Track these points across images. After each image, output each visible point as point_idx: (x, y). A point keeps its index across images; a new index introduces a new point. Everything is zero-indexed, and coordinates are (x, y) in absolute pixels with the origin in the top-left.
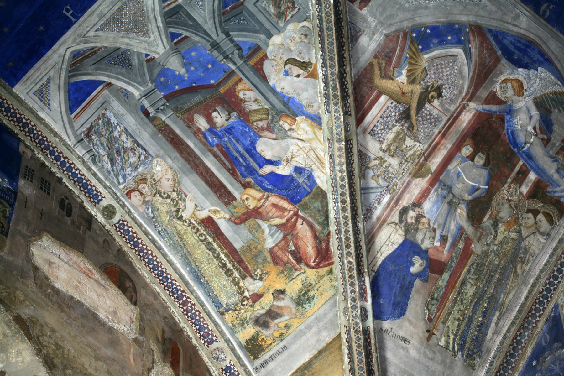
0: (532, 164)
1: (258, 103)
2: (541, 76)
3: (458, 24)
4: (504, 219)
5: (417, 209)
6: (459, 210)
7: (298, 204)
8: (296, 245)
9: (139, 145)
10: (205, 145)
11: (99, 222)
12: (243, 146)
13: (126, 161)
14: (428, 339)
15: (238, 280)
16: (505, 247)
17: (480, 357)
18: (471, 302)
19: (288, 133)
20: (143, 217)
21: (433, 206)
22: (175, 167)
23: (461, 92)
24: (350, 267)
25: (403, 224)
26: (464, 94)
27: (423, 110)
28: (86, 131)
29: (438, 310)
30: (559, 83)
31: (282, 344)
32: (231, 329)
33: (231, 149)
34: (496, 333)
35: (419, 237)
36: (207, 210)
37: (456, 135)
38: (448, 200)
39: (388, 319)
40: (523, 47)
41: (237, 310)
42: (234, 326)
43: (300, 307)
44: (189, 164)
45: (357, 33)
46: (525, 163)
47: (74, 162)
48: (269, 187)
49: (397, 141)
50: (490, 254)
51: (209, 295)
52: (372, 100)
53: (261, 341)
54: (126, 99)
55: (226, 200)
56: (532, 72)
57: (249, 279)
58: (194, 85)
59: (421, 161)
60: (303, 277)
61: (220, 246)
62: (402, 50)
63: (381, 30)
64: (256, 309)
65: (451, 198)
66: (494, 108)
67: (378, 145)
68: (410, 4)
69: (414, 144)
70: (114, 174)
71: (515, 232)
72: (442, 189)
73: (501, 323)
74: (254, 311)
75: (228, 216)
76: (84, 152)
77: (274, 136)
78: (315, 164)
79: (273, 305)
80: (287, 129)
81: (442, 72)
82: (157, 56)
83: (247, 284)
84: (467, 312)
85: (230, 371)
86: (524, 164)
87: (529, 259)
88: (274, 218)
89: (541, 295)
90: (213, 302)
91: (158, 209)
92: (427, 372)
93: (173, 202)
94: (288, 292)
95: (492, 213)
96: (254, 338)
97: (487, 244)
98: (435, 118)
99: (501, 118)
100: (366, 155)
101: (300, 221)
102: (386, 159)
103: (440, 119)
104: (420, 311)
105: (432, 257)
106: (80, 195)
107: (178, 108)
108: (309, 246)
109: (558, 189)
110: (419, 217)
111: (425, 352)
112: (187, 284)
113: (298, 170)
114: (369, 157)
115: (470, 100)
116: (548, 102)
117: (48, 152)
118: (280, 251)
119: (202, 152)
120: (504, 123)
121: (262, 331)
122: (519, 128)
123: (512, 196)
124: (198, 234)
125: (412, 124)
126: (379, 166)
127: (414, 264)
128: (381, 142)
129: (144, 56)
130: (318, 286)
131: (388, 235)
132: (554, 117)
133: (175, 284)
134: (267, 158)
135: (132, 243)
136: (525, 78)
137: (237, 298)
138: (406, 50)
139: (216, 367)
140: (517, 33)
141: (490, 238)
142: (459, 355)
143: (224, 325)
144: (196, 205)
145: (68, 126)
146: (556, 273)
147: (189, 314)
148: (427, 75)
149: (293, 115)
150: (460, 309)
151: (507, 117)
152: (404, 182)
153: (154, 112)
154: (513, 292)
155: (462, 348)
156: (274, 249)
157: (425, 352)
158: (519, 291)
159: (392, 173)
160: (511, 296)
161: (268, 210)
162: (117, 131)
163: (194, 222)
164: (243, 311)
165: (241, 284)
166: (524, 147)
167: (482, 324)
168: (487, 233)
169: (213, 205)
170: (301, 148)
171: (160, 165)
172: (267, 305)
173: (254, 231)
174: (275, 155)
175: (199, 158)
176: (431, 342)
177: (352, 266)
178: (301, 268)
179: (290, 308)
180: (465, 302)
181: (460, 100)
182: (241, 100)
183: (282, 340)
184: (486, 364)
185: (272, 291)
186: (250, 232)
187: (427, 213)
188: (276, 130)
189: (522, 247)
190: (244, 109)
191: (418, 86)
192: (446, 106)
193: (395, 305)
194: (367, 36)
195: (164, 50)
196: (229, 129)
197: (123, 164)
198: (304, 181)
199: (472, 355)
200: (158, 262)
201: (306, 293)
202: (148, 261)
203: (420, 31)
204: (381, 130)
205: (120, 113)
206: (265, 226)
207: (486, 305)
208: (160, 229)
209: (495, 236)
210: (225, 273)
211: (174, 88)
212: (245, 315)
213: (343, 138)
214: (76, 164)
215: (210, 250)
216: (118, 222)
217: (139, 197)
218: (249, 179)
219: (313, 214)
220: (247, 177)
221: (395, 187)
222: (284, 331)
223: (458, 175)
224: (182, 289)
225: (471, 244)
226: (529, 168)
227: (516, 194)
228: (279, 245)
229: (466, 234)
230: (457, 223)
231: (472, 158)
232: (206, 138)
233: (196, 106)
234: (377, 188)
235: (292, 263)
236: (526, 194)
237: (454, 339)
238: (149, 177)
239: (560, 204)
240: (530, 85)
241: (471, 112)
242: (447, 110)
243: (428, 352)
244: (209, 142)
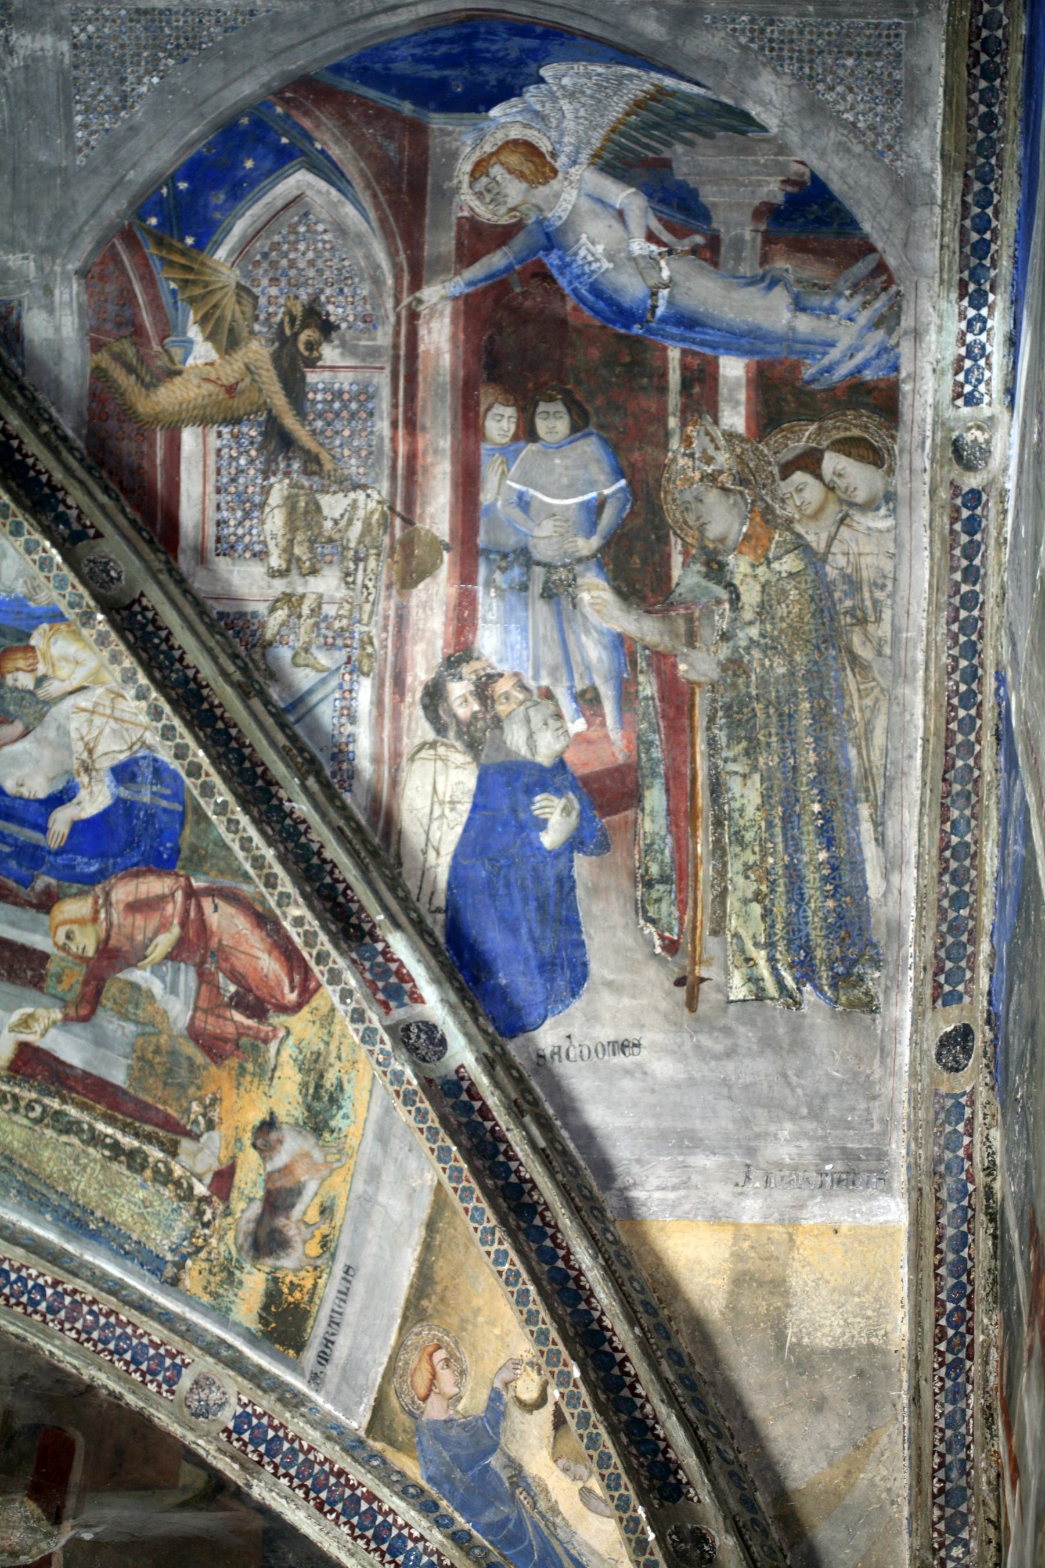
0: (711, 336)
2: (563, 87)
3: (242, 113)
4: (732, 537)
5: (466, 669)
6: (585, 597)
7: (179, 864)
8: (234, 976)
14: (692, 1003)
15: (166, 1164)
16: (782, 610)
17: (877, 963)
18: (770, 825)
21: (507, 631)
23: (377, 281)
25: (452, 734)
26: (390, 282)
27: (311, 396)
29: (682, 905)
30: (628, 70)
31: (338, 1270)
34: (891, 866)
35: (516, 739)
36: (6, 1031)
37: (442, 399)
38: (536, 588)
39: (545, 1018)
40: (456, 49)
42: (216, 1295)
43: (327, 1135)
45: (6, 318)
46: (686, 346)
49: (300, 523)
50: (747, 658)
51: (127, 1253)
52: (164, 462)
55: (29, 973)
56: (532, 95)
57: (186, 1145)
59: (398, 533)
60: (289, 1050)
61: (83, 1107)
62: (149, 281)
63: (58, 269)
64: (238, 1215)
65: (542, 578)
66: (497, 260)
67: (258, 570)
68: (86, 151)
69: (348, 501)
71: (788, 552)
72: (503, 570)
73: (891, 831)
74: (237, 1222)
75: (57, 1015)
77: (18, 727)
81: (292, 264)
84: (771, 860)
85: (250, 1423)
86: (684, 352)
87: (875, 602)
88: (151, 940)
89: (956, 676)
92: (730, 1098)
94: (282, 1115)
95: (685, 544)
96: (273, 1296)
97: (725, 637)
98: (355, 397)
99: (534, 275)
100: (242, 615)
101: (207, 904)
102: (300, 590)
103: (371, 390)
104: (630, 942)
105: (586, 771)
109: (834, 354)
110: (483, 689)
111: (698, 1047)
112: (55, 1257)
113: (124, 773)
114: (255, 614)
115: (416, 285)
116: (637, 142)
120: (554, 281)
122: (607, 265)
123: (709, 460)
124: (22, 1111)
125: (308, 452)
126: (293, 620)
127: (546, 821)
128: (261, 555)
130: (333, 1047)
131: (429, 789)
132: (685, 170)
134: (42, 795)
136: (526, 126)
137: (184, 1219)
138: (161, 274)
140: (412, 22)
141: (722, 616)
142: (806, 996)
143: (193, 1308)
146: (965, 588)
147: (95, 1335)
148: (256, 298)
149: (20, 640)
150: (745, 864)
151: (552, 260)
152: (386, 618)
154: (880, 723)
155: (806, 971)
157: (698, 1047)
158: (896, 709)
159: (339, 617)
160: (879, 738)
161: (127, 931)
164: (214, 1242)
166: (654, 307)
167: (834, 869)
168: (706, 607)
170: (93, 712)
172: (255, 1184)
173: (131, 1009)
176: (703, 1007)
177: (307, 927)
178: (275, 1029)
180: (749, 836)
181: (390, 304)
183: (333, 1256)
184: (904, 974)
185: (247, 1139)
186: (124, 1017)
187: (501, 661)
188: (12, 708)
189: (833, 582)
191: (254, 345)
192: (363, 343)
193: (547, 967)
194: (35, 311)
198: (153, 793)
199: (848, 974)
201: (319, 1086)
203: (161, 201)
204: (240, 524)
206: (140, 976)
207: (816, 808)
209: (735, 599)
210: (129, 1167)
213: (92, 603)
215: (67, 1132)
218: (43, 881)
221: (369, 650)
222: (325, 1229)
223: (523, 503)
225: (675, 666)
226: (708, 351)
227: (717, 448)
228: (201, 1004)
229: (645, 648)
230: (600, 633)
231: (527, 432)
234: (323, 682)
235: (249, 1028)
236: (748, 428)
237: (772, 960)
239: (869, 392)
240: (554, 134)
241: (442, 314)
242: (374, 352)
243: (706, 1041)
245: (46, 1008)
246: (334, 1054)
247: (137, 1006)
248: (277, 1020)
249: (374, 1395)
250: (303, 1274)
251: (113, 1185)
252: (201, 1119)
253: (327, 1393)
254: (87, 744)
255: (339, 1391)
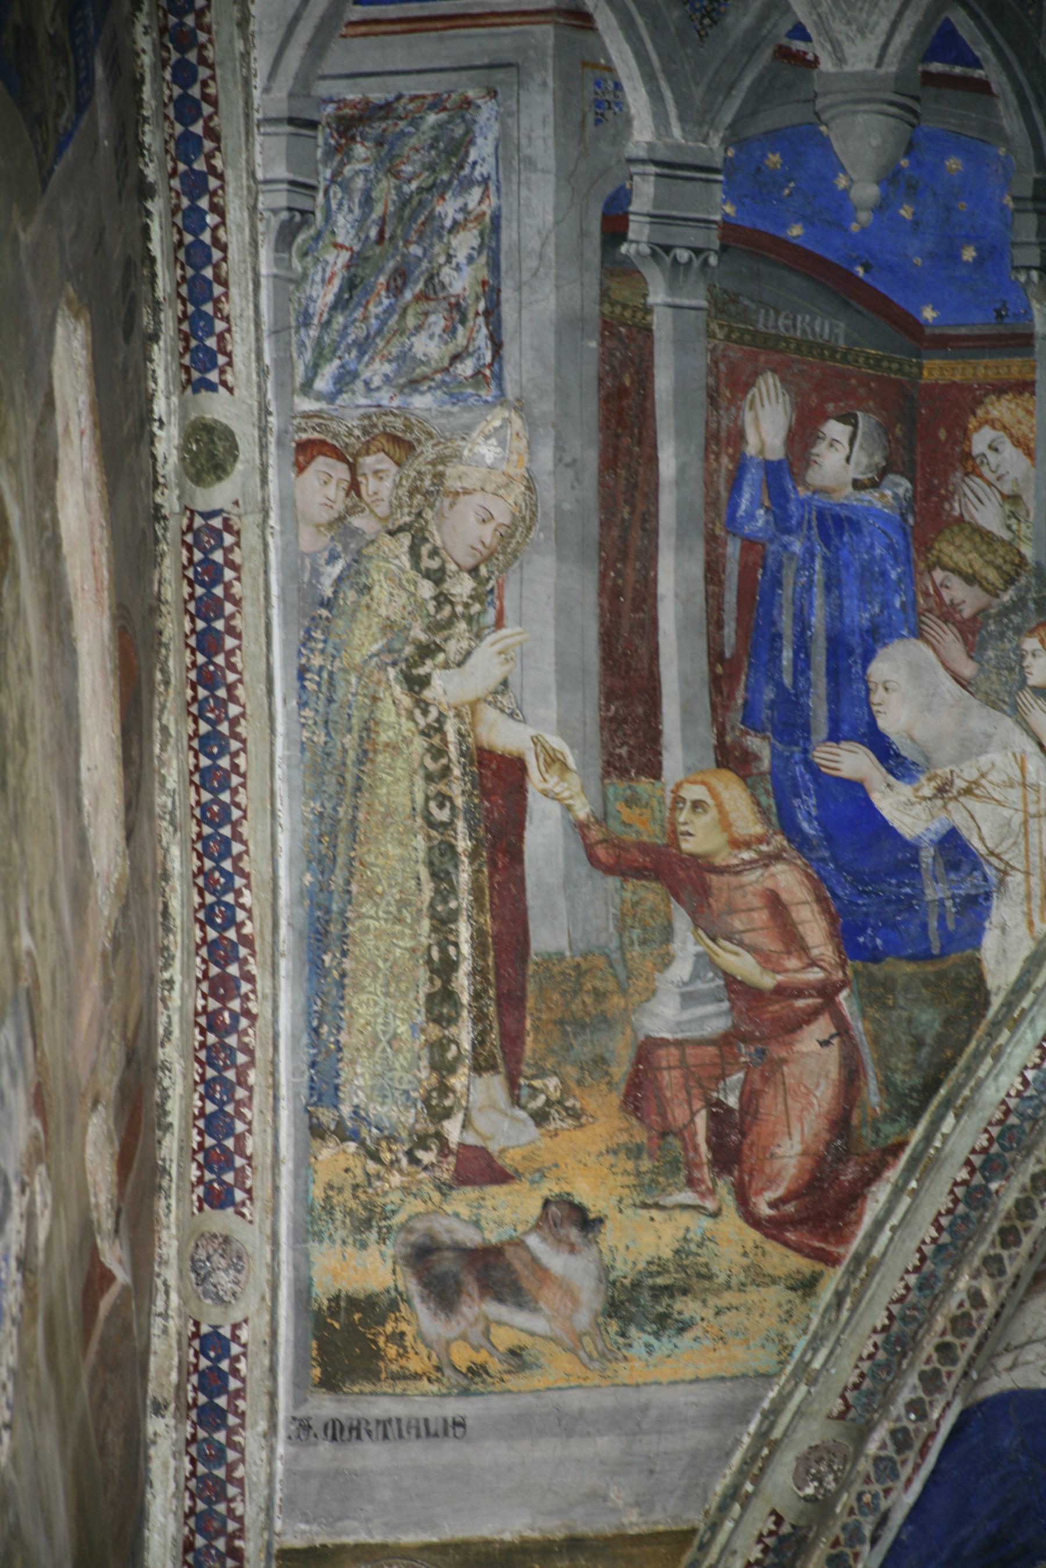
1: (1013, 515)
7: (859, 964)
8: (750, 1097)
9: (492, 314)
10: (711, 503)
11: (154, 457)
12: (836, 615)
13: (401, 331)
15: (458, 1058)
19: (1026, 698)
20: (291, 572)
22: (548, 495)
24: (967, 1316)
28: (354, 105)
31: (454, 1408)
32: (311, 1210)
33: (787, 593)
36: (531, 731)
41: (378, 1160)
42: (329, 1208)
43: (614, 1326)
44: (605, 525)
47: (229, 175)
48: (805, 825)
51: (316, 1031)
53: (389, 1339)
54: (591, 118)
55: (623, 751)
58: (860, 271)
61: (476, 890)
70: (319, 342)
74: (438, 1211)
75: (582, 811)
76: (281, 171)
77: (968, 669)
78: (1027, 874)
79: (519, 1243)
80: (1032, 681)
82: (827, 65)
83: (478, 1097)
85: (219, 1359)
88: (741, 944)
90: (313, 1065)
91: (368, 588)
93: (439, 608)
94: (609, 1236)
101: (822, 1027)
106: (165, 306)
107: (735, 302)
108: (797, 1137)
117: (175, 56)
118: (676, 1073)
119: (680, 522)
121: (417, 1302)
124: (433, 789)
129: (787, 26)
130: (730, 1298)
133: (239, 894)
135: (201, 625)
139: (184, 1300)
143: (296, 1175)
144: (505, 683)
145: (304, 33)
153: (645, 249)
156: (662, 1052)
162: (459, 202)
163: (452, 737)
165: (458, 1081)
169: (563, 729)
170: (1024, 785)
171: (502, 443)
172: (500, 1224)
173: (636, 934)
174: (917, 734)
175: (653, 534)
177: (974, 1314)
178: (712, 1192)
179: (575, 1301)
182: (968, 456)
183: (465, 1392)
185: (550, 1188)
186: (622, 928)
188: (991, 653)
190: (948, 497)
195: (871, 67)
196: (838, 520)
197: (379, 332)
198: (941, 902)
200: (235, 767)
201: (668, 1290)
202: (208, 735)
205: (526, 151)
208: (317, 661)
210: (430, 997)
211: (785, 226)
212: (395, 1197)
214: (230, 189)
215: (434, 875)
216: (207, 516)
217: (335, 492)
218: (760, 746)
219: (888, 1038)
220: (758, 729)
222: (495, 1366)
224: (247, 930)
228: (689, 1051)
232: (735, 486)
233: (798, 350)
235: (696, 1149)
238: (429, 451)
244: (734, 506)
245: (584, 788)
246: (721, 1303)
247: (643, 942)
248: (724, 1189)
249: (330, 1541)
250: (423, 1351)
251: (398, 980)
252: (541, 1100)
253: (295, 1458)
254: (976, 783)
255: (306, 1476)
